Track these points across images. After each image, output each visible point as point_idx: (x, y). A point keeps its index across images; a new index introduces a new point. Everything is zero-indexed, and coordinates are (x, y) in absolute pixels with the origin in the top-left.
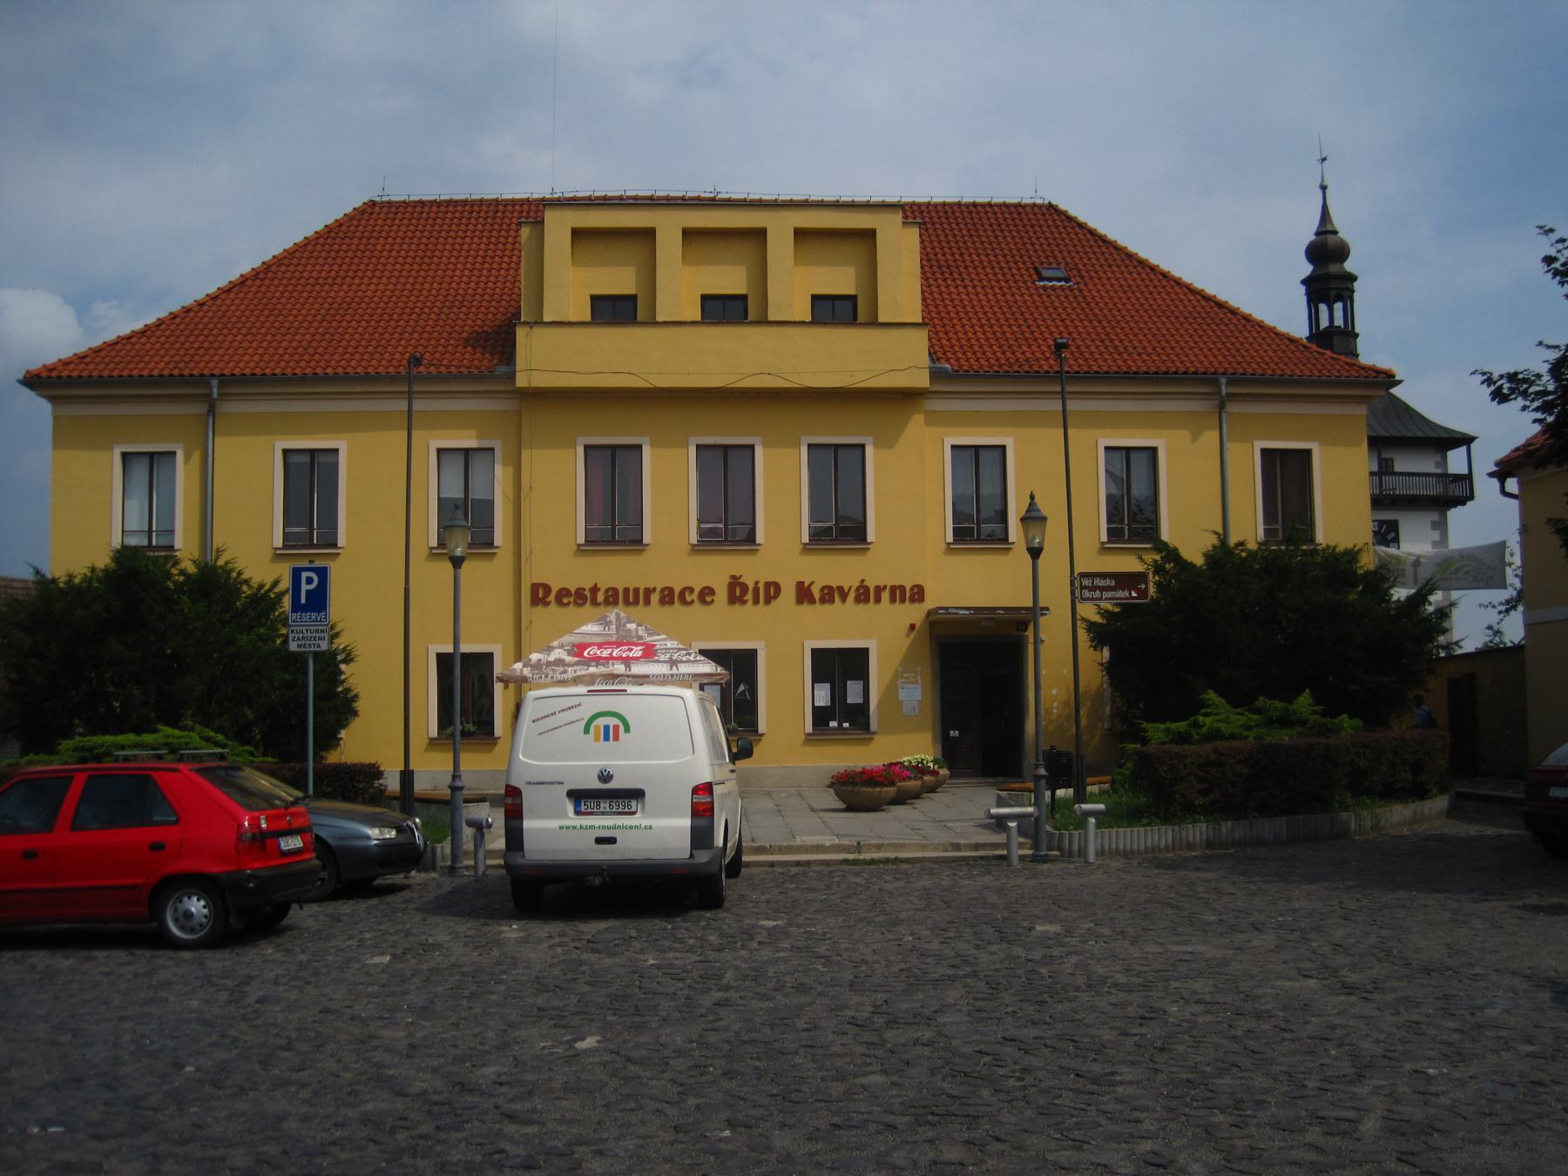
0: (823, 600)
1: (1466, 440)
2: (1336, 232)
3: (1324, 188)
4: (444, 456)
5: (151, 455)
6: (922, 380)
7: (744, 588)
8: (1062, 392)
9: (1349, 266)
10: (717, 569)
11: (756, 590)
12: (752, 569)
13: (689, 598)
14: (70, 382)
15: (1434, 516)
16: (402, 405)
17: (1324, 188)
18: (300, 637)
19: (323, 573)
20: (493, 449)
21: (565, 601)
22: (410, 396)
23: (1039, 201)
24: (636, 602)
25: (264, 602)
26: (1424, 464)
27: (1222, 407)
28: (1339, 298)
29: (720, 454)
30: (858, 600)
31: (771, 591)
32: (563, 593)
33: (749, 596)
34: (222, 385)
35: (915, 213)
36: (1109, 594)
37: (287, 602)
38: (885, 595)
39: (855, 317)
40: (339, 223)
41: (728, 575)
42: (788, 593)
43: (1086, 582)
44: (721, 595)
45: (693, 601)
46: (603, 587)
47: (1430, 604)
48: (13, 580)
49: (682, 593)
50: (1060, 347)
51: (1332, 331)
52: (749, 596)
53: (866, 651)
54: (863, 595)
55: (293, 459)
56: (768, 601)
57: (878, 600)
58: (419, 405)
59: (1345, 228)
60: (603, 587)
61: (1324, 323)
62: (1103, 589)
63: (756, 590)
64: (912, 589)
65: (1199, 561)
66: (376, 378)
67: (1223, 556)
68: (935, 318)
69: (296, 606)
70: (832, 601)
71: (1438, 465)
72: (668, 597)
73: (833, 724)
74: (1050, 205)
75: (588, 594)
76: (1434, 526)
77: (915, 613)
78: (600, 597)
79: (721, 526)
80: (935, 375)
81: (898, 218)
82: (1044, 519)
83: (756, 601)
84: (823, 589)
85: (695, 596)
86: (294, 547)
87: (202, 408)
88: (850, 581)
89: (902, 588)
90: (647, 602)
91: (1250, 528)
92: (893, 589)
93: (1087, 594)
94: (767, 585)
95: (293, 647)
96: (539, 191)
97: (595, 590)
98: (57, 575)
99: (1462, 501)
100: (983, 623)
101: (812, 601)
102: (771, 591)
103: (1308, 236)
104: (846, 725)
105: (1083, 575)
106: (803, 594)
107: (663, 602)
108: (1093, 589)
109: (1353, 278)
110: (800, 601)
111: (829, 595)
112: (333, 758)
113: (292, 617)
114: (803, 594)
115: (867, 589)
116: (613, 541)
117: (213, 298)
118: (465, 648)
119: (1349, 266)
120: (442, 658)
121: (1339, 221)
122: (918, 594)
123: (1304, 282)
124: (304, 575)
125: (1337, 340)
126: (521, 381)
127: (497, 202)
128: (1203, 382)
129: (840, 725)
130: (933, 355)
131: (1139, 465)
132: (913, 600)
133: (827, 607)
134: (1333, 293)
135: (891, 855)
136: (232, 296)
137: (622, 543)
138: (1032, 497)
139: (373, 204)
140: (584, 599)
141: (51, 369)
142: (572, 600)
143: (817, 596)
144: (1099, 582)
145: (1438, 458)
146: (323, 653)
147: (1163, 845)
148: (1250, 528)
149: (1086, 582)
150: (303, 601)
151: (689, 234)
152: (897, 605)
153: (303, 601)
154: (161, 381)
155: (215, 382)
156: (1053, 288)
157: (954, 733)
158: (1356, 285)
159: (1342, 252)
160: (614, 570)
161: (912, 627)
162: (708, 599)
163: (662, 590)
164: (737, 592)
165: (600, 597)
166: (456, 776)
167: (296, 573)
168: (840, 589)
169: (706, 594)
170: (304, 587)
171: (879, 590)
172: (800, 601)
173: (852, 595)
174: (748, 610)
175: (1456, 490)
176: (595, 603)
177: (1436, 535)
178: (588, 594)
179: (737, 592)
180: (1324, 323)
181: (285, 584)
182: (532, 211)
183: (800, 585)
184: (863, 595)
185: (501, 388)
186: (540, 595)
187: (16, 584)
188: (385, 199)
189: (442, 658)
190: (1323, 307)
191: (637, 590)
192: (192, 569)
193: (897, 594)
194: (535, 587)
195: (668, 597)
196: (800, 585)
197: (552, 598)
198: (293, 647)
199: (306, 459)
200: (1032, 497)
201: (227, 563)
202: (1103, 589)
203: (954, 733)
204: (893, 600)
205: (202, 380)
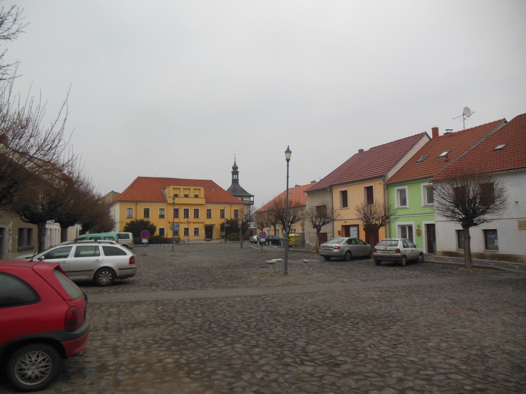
1: (253, 196)
6: (204, 203)
9: (238, 170)
10: (186, 220)
20: (164, 209)
42: (192, 223)
68: (205, 197)
77: (203, 224)
80: (206, 203)
82: (291, 152)
88: (198, 221)
91: (233, 217)
98: (500, 248)
99: (252, 204)
103: (233, 165)
106: (193, 223)
111: (196, 223)
114: (193, 223)
119: (238, 170)
122: (204, 223)
138: (288, 147)
157: (145, 241)
159: (237, 168)
169: (185, 223)
175: (251, 203)
180: (234, 178)
190: (234, 175)
193: (202, 223)
200: (288, 147)
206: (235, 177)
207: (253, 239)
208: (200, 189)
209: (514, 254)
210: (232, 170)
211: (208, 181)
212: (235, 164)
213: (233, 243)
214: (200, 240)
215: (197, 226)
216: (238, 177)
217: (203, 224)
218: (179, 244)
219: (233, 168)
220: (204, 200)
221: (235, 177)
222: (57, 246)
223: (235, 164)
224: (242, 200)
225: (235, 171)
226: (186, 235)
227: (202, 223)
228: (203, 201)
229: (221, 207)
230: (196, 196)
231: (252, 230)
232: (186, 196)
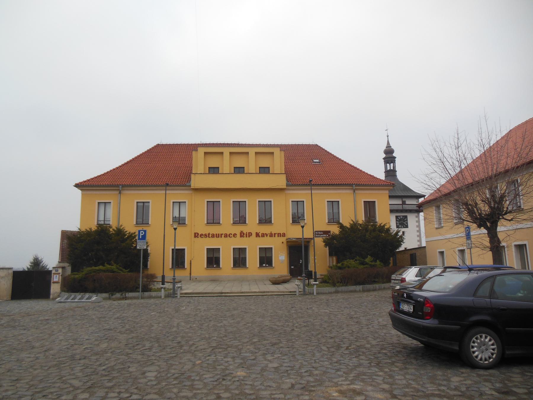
0: (262, 236)
2: (391, 147)
3: (388, 136)
4: (175, 204)
5: (105, 203)
7: (244, 233)
8: (311, 189)
9: (394, 155)
10: (238, 229)
11: (246, 234)
12: (245, 229)
13: (231, 236)
14: (86, 186)
15: (416, 214)
16: (164, 192)
17: (388, 136)
18: (141, 245)
19: (145, 231)
21: (202, 237)
22: (166, 190)
23: (314, 144)
24: (219, 237)
25: (132, 236)
26: (413, 202)
27: (354, 192)
28: (392, 162)
29: (238, 203)
30: (270, 236)
31: (250, 234)
32: (201, 235)
33: (245, 236)
34: (122, 187)
35: (283, 147)
36: (322, 236)
37: (137, 238)
38: (276, 235)
39: (269, 172)
40: (150, 149)
41: (195, 238)
42: (254, 235)
43: (316, 233)
44: (238, 235)
45: (232, 237)
46: (211, 233)
47: (399, 235)
48: (68, 231)
49: (229, 235)
50: (311, 181)
51: (390, 170)
52: (245, 236)
53: (184, 249)
54: (271, 235)
55: (139, 204)
56: (249, 237)
57: (275, 236)
58: (168, 192)
59: (393, 147)
60: (211, 233)
61: (388, 169)
62: (320, 234)
63: (246, 234)
64: (283, 234)
65: (348, 226)
66: (159, 186)
67: (354, 226)
69: (139, 239)
70: (264, 237)
71: (417, 202)
72: (226, 236)
73: (264, 265)
74: (316, 145)
75: (208, 235)
76: (417, 217)
77: (284, 239)
78: (210, 236)
79: (239, 219)
81: (279, 149)
83: (246, 237)
84: (262, 234)
85: (232, 236)
86: (139, 224)
87: (118, 192)
88: (268, 232)
89: (280, 234)
90: (221, 237)
91: (361, 218)
92: (278, 234)
93: (317, 236)
94: (249, 233)
95: (138, 248)
96: (198, 142)
97: (209, 234)
100: (299, 242)
101: (259, 237)
102: (250, 234)
103: (384, 148)
104: (267, 265)
105: (316, 231)
106: (257, 235)
107: (225, 237)
108: (318, 234)
109: (395, 158)
110: (256, 237)
111: (263, 235)
112: (146, 272)
113: (138, 241)
114: (257, 235)
115: (272, 234)
116: (213, 223)
117: (120, 166)
118: (176, 248)
119: (394, 155)
120: (173, 249)
121: (391, 145)
122: (284, 235)
123: (383, 159)
124: (141, 232)
125: (391, 174)
126: (193, 186)
127: (188, 144)
128: (349, 186)
129: (266, 265)
130: (287, 180)
131: (335, 205)
132: (283, 236)
133: (263, 238)
134: (390, 161)
135: (271, 294)
136: (125, 166)
137: (215, 223)
139: (158, 145)
140: (207, 236)
141: (81, 183)
142: (204, 236)
143: (260, 235)
144: (319, 233)
145: (417, 200)
146: (145, 249)
147: (332, 292)
148: (361, 218)
149: (316, 233)
150: (141, 238)
151: (231, 153)
152: (279, 237)
153: (141, 238)
154: (108, 186)
155: (121, 186)
156: (316, 164)
157: (292, 267)
158: (396, 159)
159: (392, 151)
160: (214, 229)
161: (283, 243)
162: (235, 236)
163: (225, 234)
164: (242, 235)
165: (210, 236)
166: (174, 276)
167: (139, 231)
168: (266, 234)
169: (235, 235)
170: (141, 234)
171: (275, 234)
172: (256, 237)
173: (269, 235)
174: (245, 239)
176: (209, 237)
177: (417, 219)
178: (208, 235)
179: (242, 235)
180: (388, 169)
181: (137, 233)
182: (195, 147)
183: (257, 233)
184: (271, 235)
185: (188, 188)
186: (196, 235)
187: (68, 232)
188: (162, 143)
189: (173, 249)
191: (219, 234)
192: (115, 229)
193: (279, 235)
194: (195, 234)
195: (226, 236)
196: (257, 233)
197: (199, 236)
198: (138, 248)
199: (142, 204)
201: (123, 228)
202: (320, 234)
203: (292, 267)
204: (278, 236)
205: (118, 186)
206: (390, 167)
207: (403, 280)
208: (273, 153)
209: (463, 279)
210: (384, 156)
211: (308, 146)
212: (388, 146)
213: (337, 292)
214: (53, 279)
215: (266, 243)
216: (394, 167)
217: (284, 239)
218: (146, 294)
219: (386, 152)
220: (284, 177)
221: (390, 167)
222: (142, 280)
223: (388, 146)
224: (404, 203)
225: (390, 156)
226: (239, 266)
227: (279, 235)
228: (281, 181)
229: (333, 195)
230: (264, 170)
231: (414, 252)
232: (239, 170)
